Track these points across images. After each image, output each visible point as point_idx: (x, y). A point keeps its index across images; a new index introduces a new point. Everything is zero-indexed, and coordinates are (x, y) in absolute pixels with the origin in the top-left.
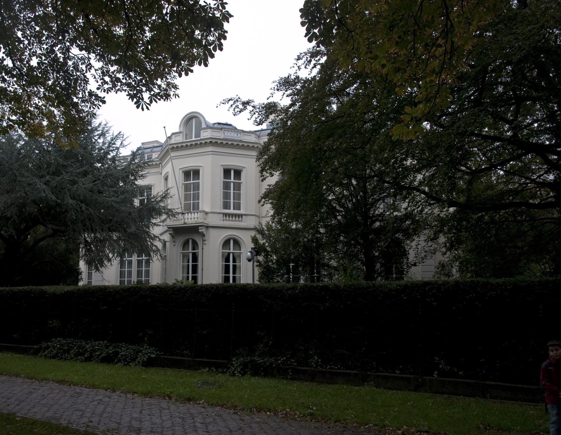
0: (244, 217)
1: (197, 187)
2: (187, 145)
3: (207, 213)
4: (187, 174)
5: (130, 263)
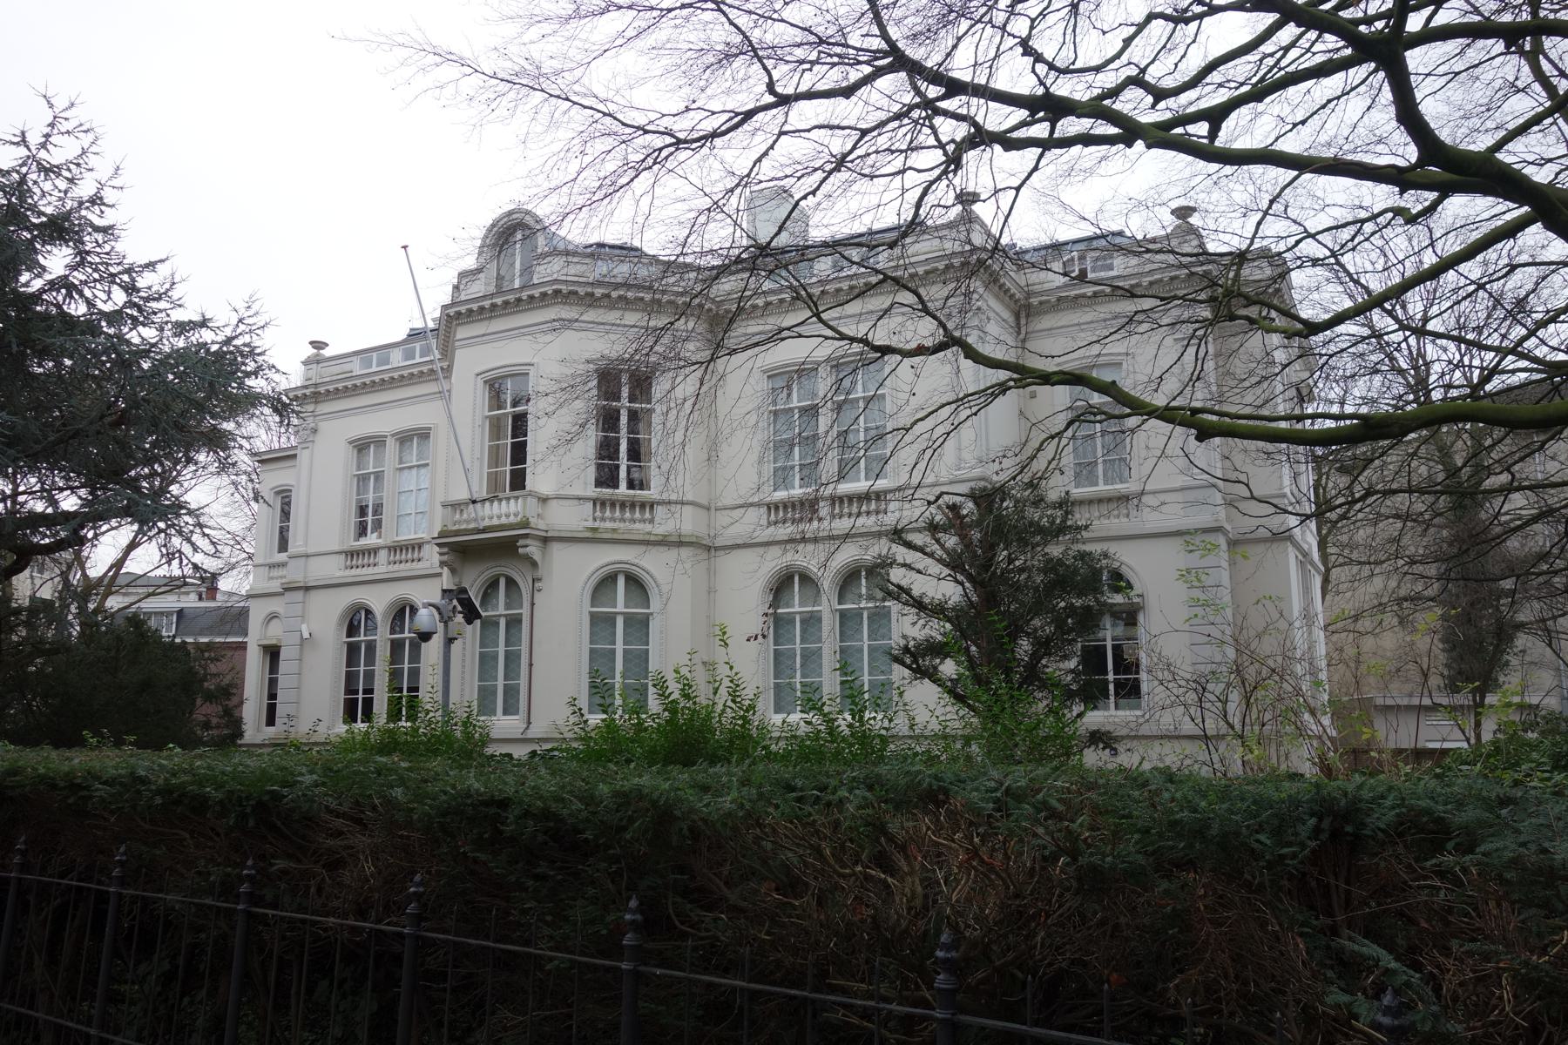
2: (470, 311)
3: (544, 500)
5: (811, 621)
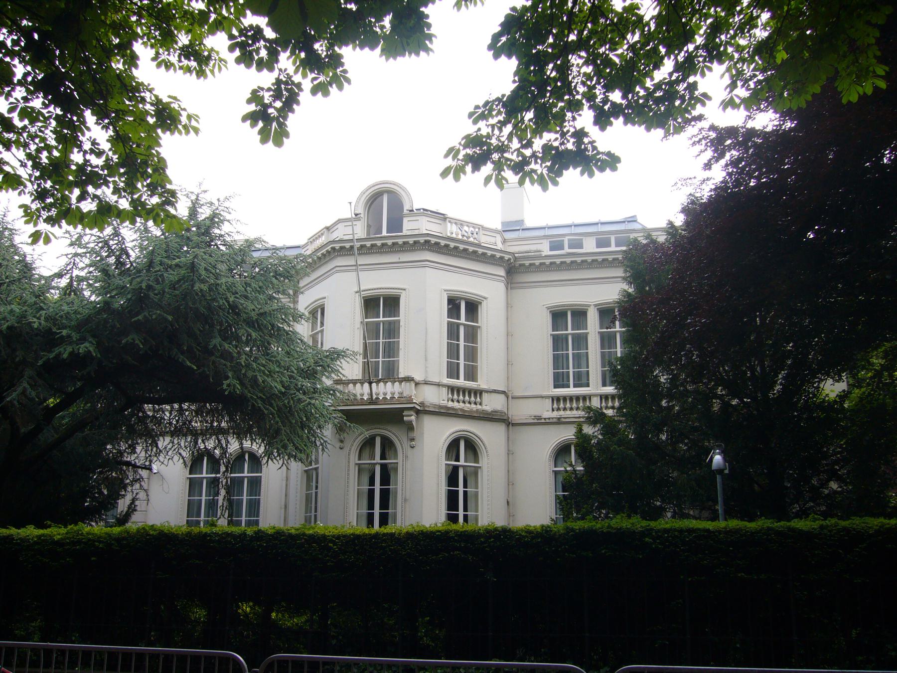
0: (485, 395)
1: (393, 330)
4: (370, 304)
